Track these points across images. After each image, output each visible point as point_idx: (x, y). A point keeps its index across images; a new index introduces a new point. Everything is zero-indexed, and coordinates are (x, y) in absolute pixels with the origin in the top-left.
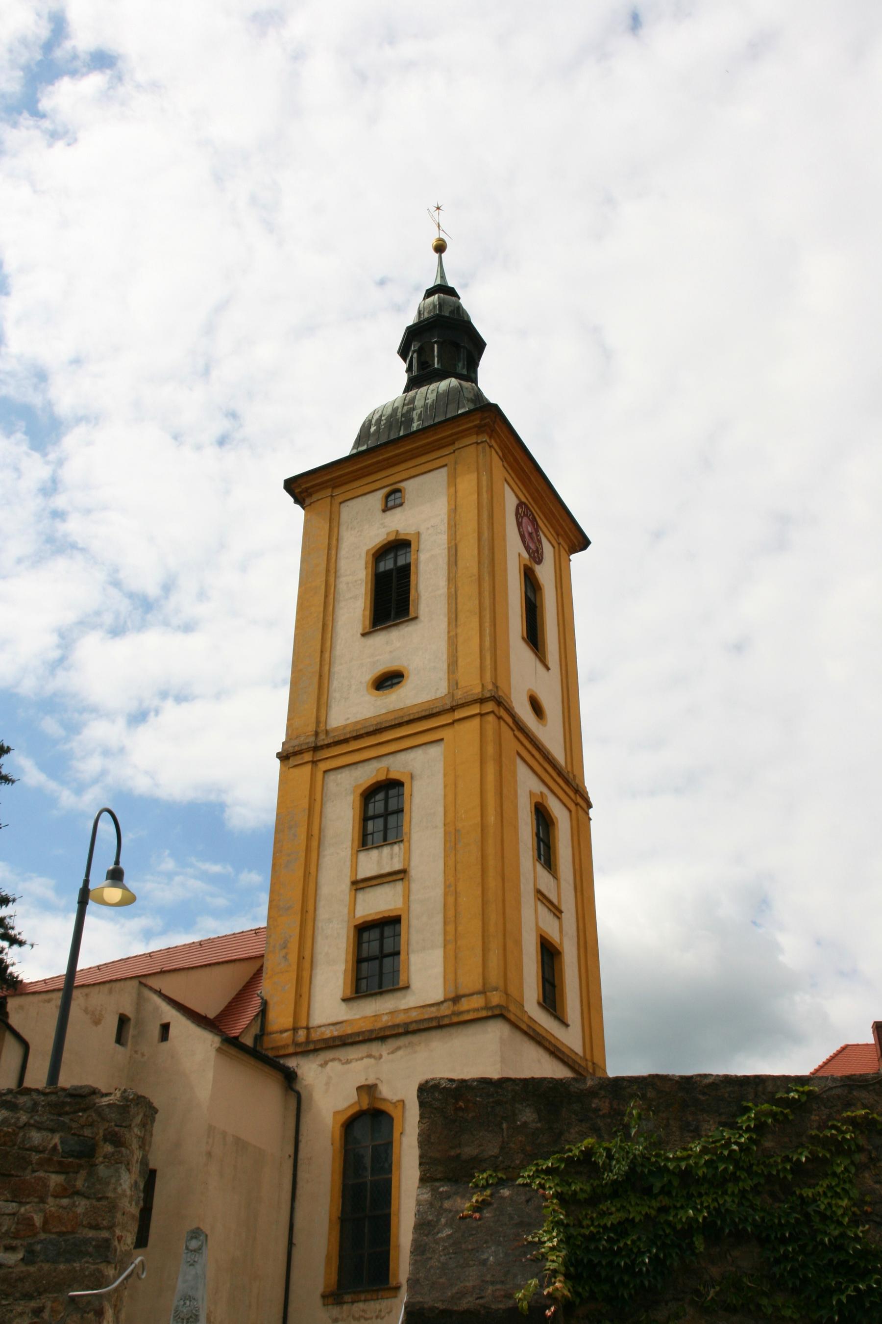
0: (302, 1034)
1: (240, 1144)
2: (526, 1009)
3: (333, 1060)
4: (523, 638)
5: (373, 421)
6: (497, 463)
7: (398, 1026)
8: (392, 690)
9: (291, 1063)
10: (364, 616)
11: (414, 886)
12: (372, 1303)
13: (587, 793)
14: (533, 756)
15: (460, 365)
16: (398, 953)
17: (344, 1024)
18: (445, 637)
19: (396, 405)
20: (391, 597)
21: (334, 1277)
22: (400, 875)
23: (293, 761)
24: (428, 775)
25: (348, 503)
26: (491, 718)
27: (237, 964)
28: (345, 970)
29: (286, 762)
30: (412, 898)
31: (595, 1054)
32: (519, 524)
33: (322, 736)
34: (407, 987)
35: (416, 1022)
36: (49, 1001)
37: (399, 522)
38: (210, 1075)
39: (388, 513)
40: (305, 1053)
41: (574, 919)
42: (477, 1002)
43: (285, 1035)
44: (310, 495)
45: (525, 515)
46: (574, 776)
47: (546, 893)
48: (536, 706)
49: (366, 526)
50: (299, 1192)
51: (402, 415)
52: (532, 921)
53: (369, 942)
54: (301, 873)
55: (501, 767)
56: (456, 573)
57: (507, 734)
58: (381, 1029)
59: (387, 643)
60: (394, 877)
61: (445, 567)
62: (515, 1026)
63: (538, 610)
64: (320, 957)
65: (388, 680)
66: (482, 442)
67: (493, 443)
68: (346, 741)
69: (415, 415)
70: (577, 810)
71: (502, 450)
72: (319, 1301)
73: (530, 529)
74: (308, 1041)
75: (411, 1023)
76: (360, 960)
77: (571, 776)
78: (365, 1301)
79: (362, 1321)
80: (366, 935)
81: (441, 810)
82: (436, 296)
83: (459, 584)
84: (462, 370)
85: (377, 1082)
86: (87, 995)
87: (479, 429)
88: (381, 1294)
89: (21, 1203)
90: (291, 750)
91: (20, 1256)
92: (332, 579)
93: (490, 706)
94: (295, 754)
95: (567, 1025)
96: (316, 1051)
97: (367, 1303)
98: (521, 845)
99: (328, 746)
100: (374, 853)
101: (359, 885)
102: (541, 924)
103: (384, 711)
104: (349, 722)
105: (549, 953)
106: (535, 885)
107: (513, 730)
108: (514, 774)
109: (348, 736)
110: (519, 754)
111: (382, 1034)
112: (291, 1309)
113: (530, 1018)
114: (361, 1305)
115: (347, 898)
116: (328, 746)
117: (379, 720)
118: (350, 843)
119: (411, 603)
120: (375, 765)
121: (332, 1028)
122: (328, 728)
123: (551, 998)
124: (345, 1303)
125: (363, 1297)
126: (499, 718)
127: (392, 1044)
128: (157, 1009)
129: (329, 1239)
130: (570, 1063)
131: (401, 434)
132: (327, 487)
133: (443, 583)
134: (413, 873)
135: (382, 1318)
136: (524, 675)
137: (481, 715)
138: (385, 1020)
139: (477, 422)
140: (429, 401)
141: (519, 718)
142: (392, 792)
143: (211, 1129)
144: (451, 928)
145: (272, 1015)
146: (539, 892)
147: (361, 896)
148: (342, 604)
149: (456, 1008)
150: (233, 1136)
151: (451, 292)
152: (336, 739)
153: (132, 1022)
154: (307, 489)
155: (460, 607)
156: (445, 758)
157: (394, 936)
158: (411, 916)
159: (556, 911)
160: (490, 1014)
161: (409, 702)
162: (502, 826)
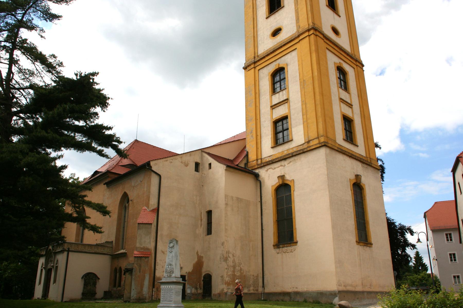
0: (259, 161)
3: (270, 168)
4: (327, 6)
9: (257, 171)
11: (291, 104)
14: (334, 49)
18: (294, 10)
21: (276, 240)
22: (286, 101)
23: (248, 69)
24: (292, 62)
26: (313, 36)
30: (291, 108)
33: (256, 58)
36: (167, 161)
38: (224, 178)
42: (316, 142)
47: (345, 99)
50: (263, 213)
52: (338, 110)
57: (321, 41)
58: (284, 156)
64: (263, 135)
65: (276, 32)
68: (264, 57)
70: (357, 68)
72: (272, 247)
74: (262, 163)
77: (354, 55)
88: (291, 244)
93: (312, 32)
94: (249, 66)
95: (358, 146)
96: (264, 166)
99: (259, 61)
100: (277, 95)
102: (343, 111)
105: (348, 122)
106: (339, 96)
110: (327, 48)
112: (264, 250)
114: (285, 248)
115: (270, 112)
116: (259, 61)
120: (274, 63)
123: (350, 136)
125: (286, 246)
126: (316, 35)
128: (207, 158)
130: (359, 159)
137: (309, 36)
138: (286, 153)
141: (326, 35)
143: (226, 196)
144: (305, 117)
145: (250, 156)
146: (341, 99)
147: (274, 110)
159: (350, 105)
160: (321, 145)
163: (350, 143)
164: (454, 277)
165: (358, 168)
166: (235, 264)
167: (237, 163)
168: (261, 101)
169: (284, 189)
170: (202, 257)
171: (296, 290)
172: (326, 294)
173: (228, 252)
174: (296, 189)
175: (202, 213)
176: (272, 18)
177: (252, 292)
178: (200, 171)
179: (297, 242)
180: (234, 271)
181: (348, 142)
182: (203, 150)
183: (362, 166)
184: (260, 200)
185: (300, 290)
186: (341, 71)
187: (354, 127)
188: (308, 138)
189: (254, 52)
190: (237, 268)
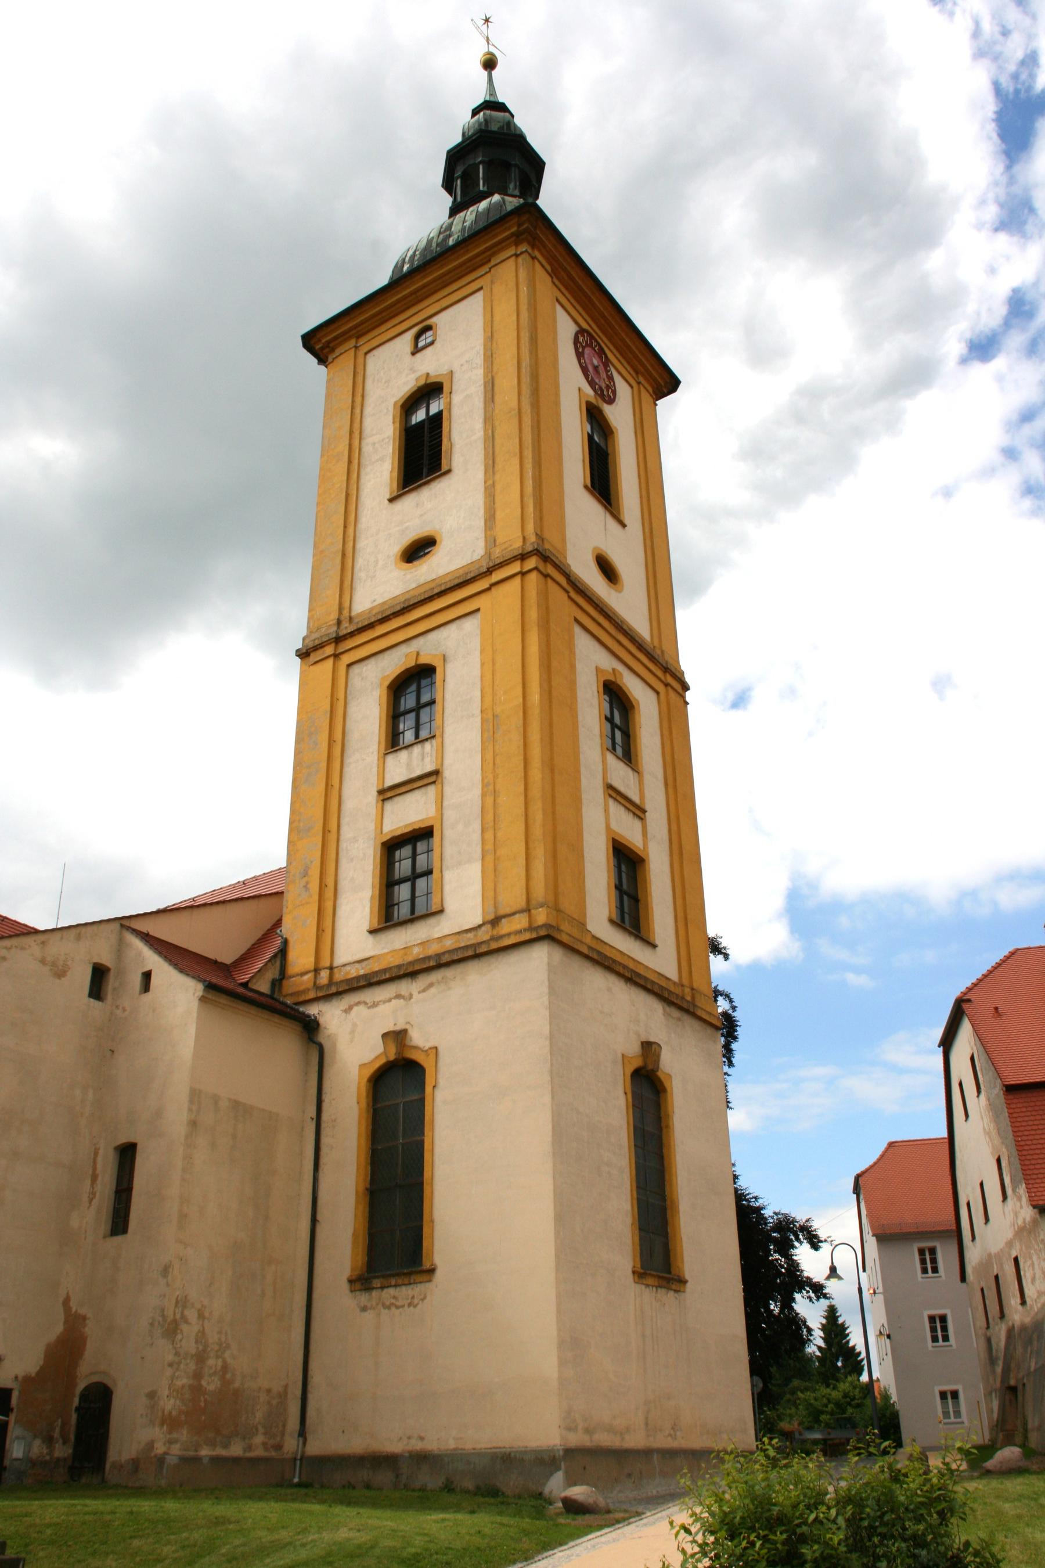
0: (324, 975)
1: (239, 1109)
2: (589, 928)
3: (358, 1003)
5: (407, 259)
9: (313, 1010)
11: (448, 790)
12: (404, 1288)
13: (683, 673)
14: (599, 624)
15: (512, 186)
17: (371, 961)
20: (421, 455)
21: (362, 1259)
23: (314, 657)
24: (463, 654)
25: (375, 352)
26: (533, 576)
28: (372, 897)
29: (307, 659)
30: (445, 803)
31: (694, 978)
32: (579, 355)
33: (345, 624)
34: (441, 911)
35: (449, 952)
37: (430, 364)
38: (192, 1029)
39: (418, 355)
40: (328, 997)
41: (665, 821)
42: (520, 922)
43: (306, 977)
44: (333, 350)
45: (587, 345)
46: (663, 652)
47: (622, 789)
48: (606, 568)
49: (392, 370)
50: (323, 1160)
51: (437, 245)
52: (598, 824)
53: (400, 861)
55: (548, 636)
56: (493, 410)
58: (410, 963)
60: (426, 781)
61: (482, 405)
62: (570, 949)
63: (610, 457)
64: (344, 884)
65: (418, 550)
66: (522, 253)
67: (537, 253)
68: (370, 626)
72: (345, 1286)
73: (595, 362)
74: (331, 982)
75: (444, 953)
76: (389, 883)
77: (658, 652)
78: (396, 1286)
79: (393, 1309)
81: (478, 694)
82: (482, 114)
83: (497, 423)
85: (407, 1027)
86: (43, 943)
87: (517, 239)
88: (413, 1278)
90: (311, 645)
92: (356, 442)
93: (532, 563)
94: (316, 648)
95: (654, 946)
96: (339, 994)
97: (398, 1289)
98: (582, 732)
100: (403, 755)
101: (387, 794)
102: (614, 826)
103: (414, 586)
104: (376, 603)
105: (627, 862)
106: (604, 778)
107: (567, 592)
109: (373, 620)
110: (576, 620)
111: (411, 969)
113: (594, 937)
114: (391, 1291)
116: (352, 634)
117: (407, 596)
118: (376, 747)
119: (443, 454)
120: (404, 649)
121: (357, 965)
123: (631, 912)
124: (373, 1288)
125: (393, 1282)
126: (546, 576)
127: (423, 981)
129: (356, 1216)
132: (350, 338)
133: (478, 425)
134: (447, 773)
135: (415, 1306)
136: (585, 530)
137: (523, 574)
138: (417, 952)
139: (514, 229)
140: (467, 224)
143: (195, 1095)
144: (489, 835)
146: (610, 787)
147: (388, 806)
148: (368, 469)
149: (495, 932)
150: (230, 1100)
151: (502, 107)
152: (360, 625)
153: (112, 974)
154: (329, 342)
155: (497, 449)
156: (481, 631)
157: (428, 852)
158: (444, 824)
159: (638, 811)
160: (534, 935)
161: (442, 572)
162: (550, 706)
163: (630, 933)
164: (943, 1395)
165: (651, 1019)
166: (206, 1346)
167: (245, 978)
169: (400, 1079)
170: (84, 1318)
171: (417, 1445)
173: (182, 1302)
174: (442, 1082)
175: (101, 1152)
176: (409, 502)
177: (259, 1452)
178: (109, 997)
179: (432, 1271)
180: (198, 1375)
181: (625, 929)
182: (126, 923)
184: (314, 1115)
185: (432, 1445)
187: (645, 881)
188: (495, 907)
190: (211, 1362)
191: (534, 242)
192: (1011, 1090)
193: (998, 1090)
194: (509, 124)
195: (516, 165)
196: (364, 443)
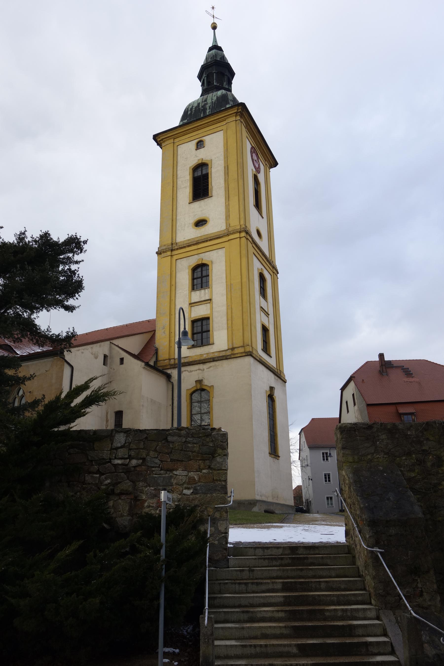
4: (254, 205)
5: (189, 109)
6: (244, 129)
7: (210, 358)
8: (202, 227)
9: (169, 371)
10: (189, 195)
15: (225, 83)
16: (209, 331)
19: (199, 102)
20: (201, 187)
23: (163, 255)
24: (219, 262)
27: (144, 334)
33: (174, 245)
37: (202, 155)
42: (241, 350)
43: (166, 361)
49: (188, 155)
51: (202, 107)
52: (260, 318)
54: (168, 300)
57: (250, 245)
59: (200, 207)
65: (200, 223)
67: (242, 120)
69: (207, 107)
71: (245, 123)
80: (195, 324)
81: (225, 276)
82: (214, 50)
84: (225, 85)
89: (189, 472)
91: (192, 491)
93: (243, 234)
94: (164, 252)
95: (271, 357)
100: (198, 292)
102: (262, 320)
105: (265, 330)
108: (253, 261)
111: (204, 361)
116: (177, 249)
118: (188, 289)
122: (177, 242)
126: (247, 239)
127: (208, 365)
131: (202, 116)
133: (222, 181)
136: (255, 222)
138: (205, 356)
140: (214, 101)
142: (204, 268)
144: (230, 322)
146: (261, 307)
147: (193, 308)
149: (233, 352)
151: (220, 49)
153: (109, 357)
159: (267, 314)
160: (246, 354)
164: (328, 498)
168: (177, 295)
172: (244, 503)
175: (109, 413)
176: (197, 204)
183: (275, 378)
184: (171, 404)
186: (262, 278)
189: (172, 238)
191: (242, 116)
192: (368, 405)
193: (364, 405)
194: (223, 57)
195: (226, 75)
196: (178, 180)
